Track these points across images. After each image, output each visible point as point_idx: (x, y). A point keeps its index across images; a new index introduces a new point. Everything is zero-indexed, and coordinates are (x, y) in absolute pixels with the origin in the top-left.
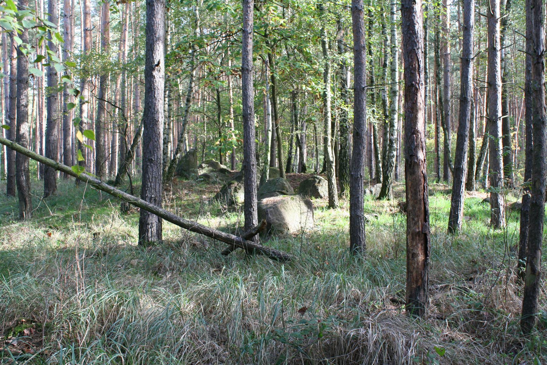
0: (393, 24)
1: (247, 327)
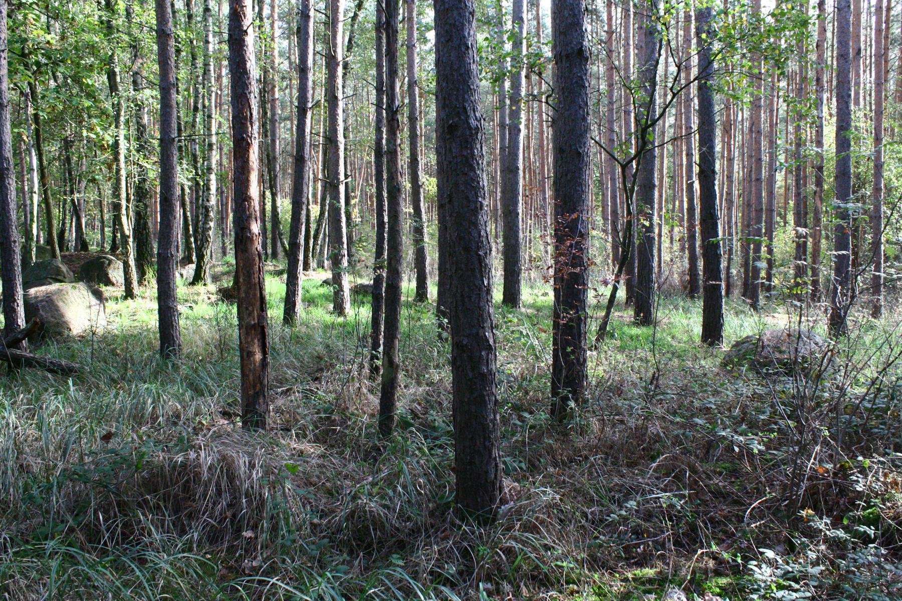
0: (206, 56)
1: (23, 469)
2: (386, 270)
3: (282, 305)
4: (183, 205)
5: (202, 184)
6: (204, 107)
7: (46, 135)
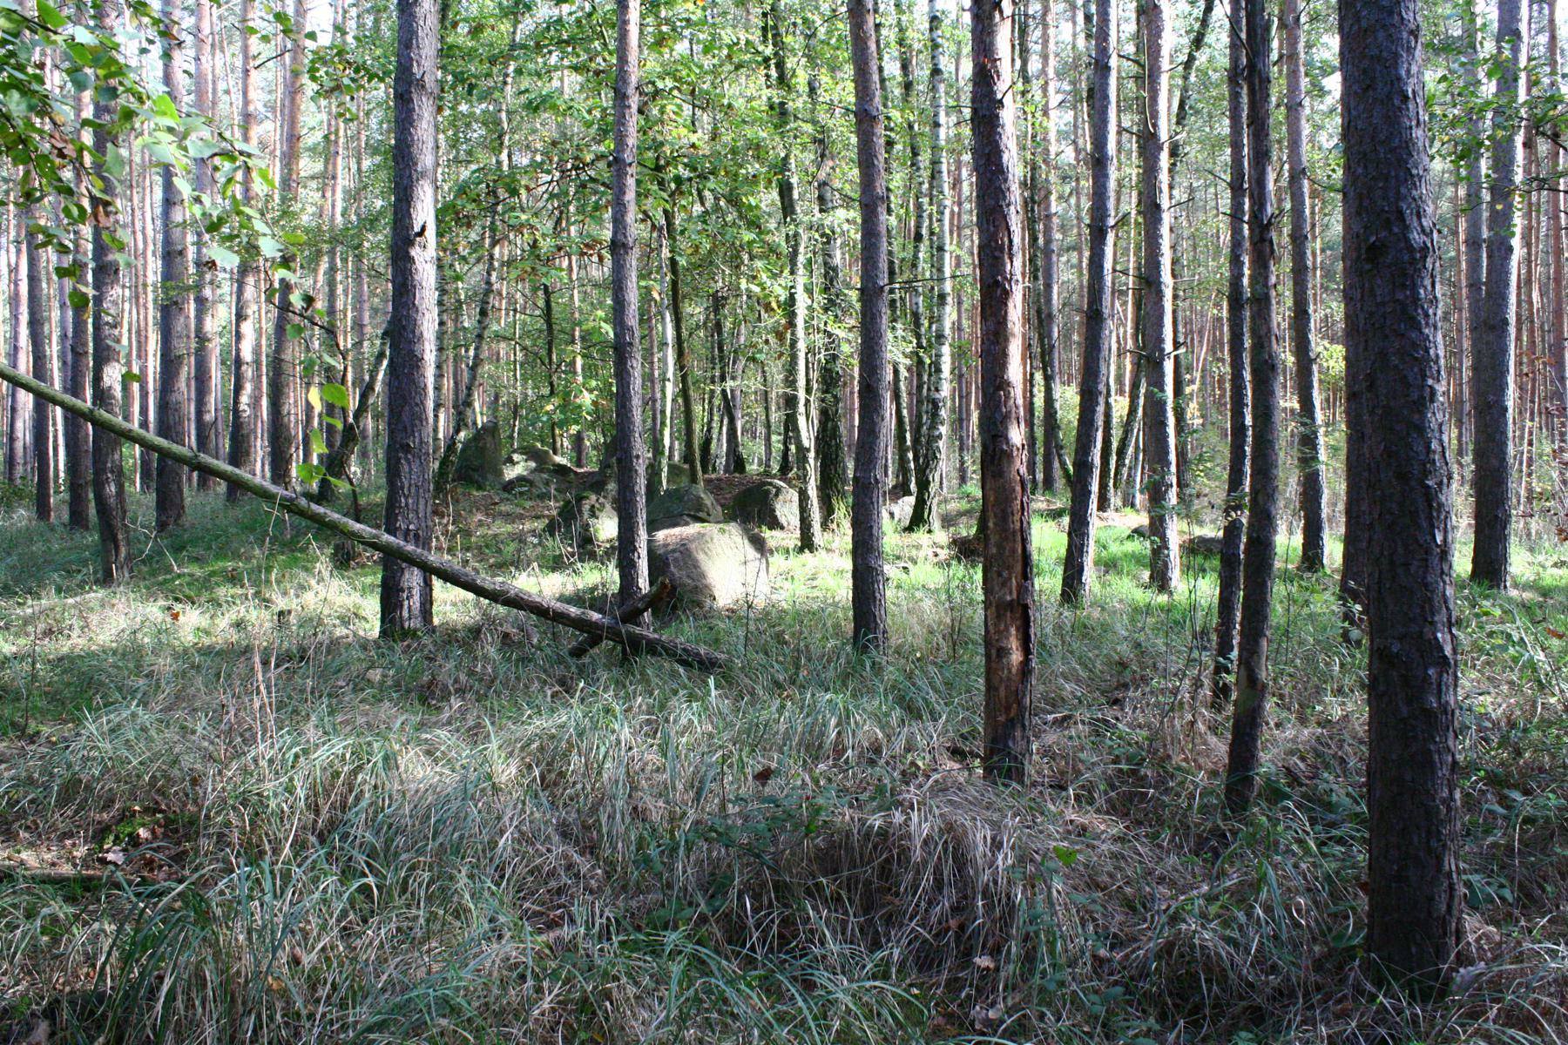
0: (935, 148)
1: (638, 813)
2: (1247, 512)
3: (1060, 571)
4: (897, 396)
5: (928, 361)
6: (932, 233)
7: (686, 290)
